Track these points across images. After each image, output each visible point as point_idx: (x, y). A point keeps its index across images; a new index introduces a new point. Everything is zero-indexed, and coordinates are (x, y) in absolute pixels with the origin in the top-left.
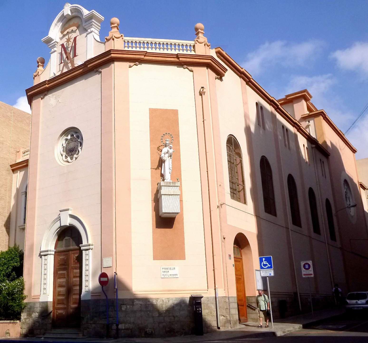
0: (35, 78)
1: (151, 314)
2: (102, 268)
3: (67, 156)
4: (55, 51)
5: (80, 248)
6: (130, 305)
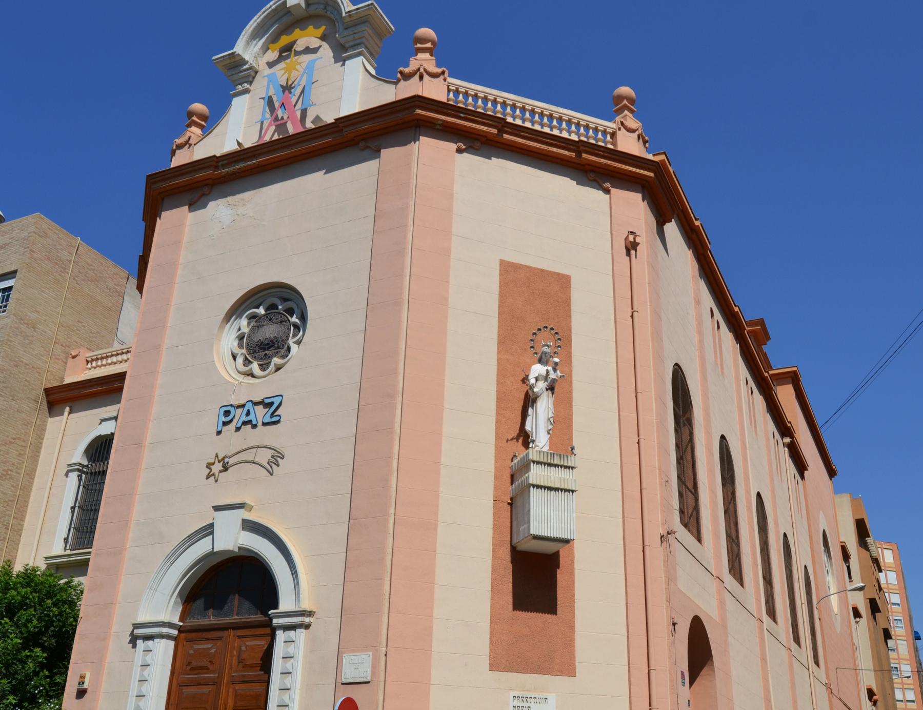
0: (177, 151)
3: (249, 358)
4: (246, 91)
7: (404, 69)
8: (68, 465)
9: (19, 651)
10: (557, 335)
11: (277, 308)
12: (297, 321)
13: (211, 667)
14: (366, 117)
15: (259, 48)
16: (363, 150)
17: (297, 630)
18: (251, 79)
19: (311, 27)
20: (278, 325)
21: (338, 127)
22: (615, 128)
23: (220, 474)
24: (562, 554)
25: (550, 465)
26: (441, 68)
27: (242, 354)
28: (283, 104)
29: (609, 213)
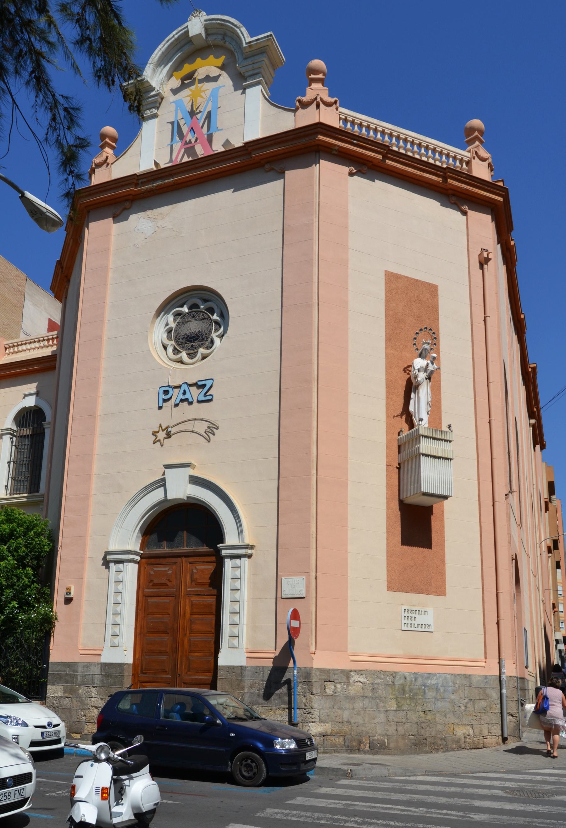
0: (96, 169)
1: (381, 704)
2: (280, 601)
3: (178, 348)
4: (155, 116)
5: (218, 551)
6: (343, 684)
7: (303, 98)
8: (2, 430)
9: (15, 568)
10: (434, 335)
11: (199, 307)
12: (218, 318)
13: (169, 584)
14: (272, 142)
15: (164, 75)
16: (267, 172)
17: (242, 559)
18: (158, 105)
19: (211, 57)
20: (201, 322)
21: (247, 150)
22: (470, 157)
23: (165, 440)
24: (435, 507)
25: (434, 439)
26: (333, 98)
27: (172, 344)
28: (192, 128)
29: (466, 232)
